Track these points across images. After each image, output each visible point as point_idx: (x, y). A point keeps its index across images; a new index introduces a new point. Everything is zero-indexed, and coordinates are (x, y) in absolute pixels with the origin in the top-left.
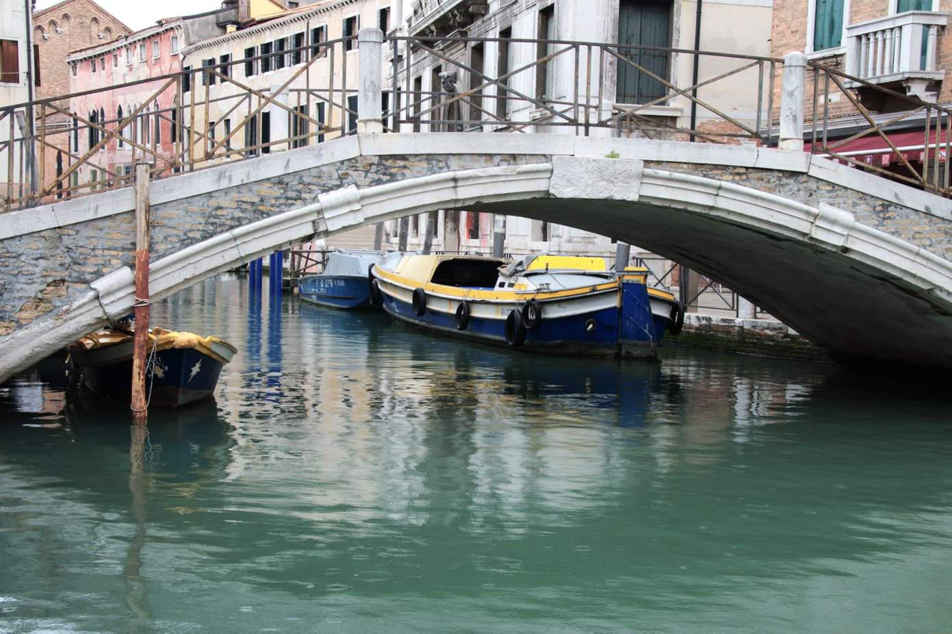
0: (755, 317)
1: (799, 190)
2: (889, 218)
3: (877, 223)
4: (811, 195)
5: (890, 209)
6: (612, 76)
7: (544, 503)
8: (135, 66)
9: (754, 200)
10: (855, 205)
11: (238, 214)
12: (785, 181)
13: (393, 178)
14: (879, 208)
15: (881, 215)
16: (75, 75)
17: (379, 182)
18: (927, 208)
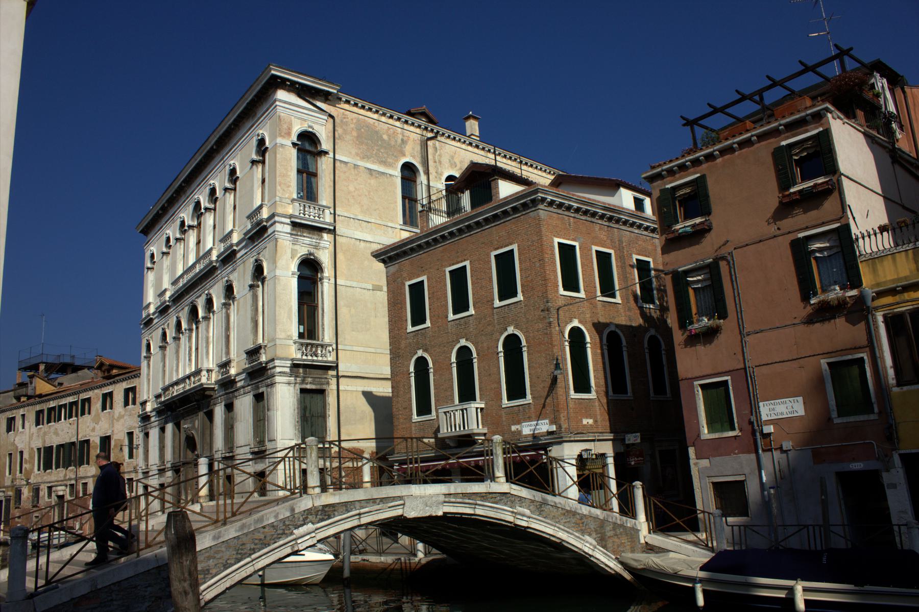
10: (529, 506)
17: (322, 520)
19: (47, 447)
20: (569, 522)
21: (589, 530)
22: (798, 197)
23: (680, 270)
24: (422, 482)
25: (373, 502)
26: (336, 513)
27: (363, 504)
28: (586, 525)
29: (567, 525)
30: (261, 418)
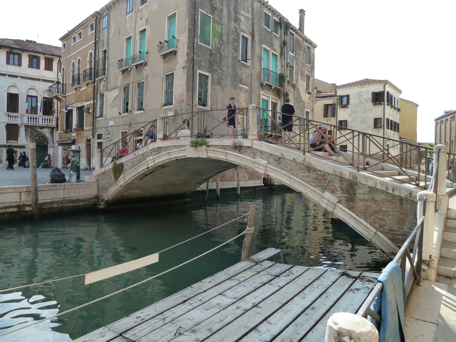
0: (29, 167)
1: (251, 153)
2: (280, 163)
3: (276, 165)
4: (254, 154)
5: (281, 159)
7: (118, 238)
9: (276, 172)
10: (269, 158)
12: (246, 150)
14: (277, 159)
15: (278, 162)
17: (157, 154)
18: (294, 159)
19: (51, 115)
20: (308, 176)
21: (332, 188)
22: (140, 192)
23: (262, 61)
24: (81, 309)
25: (175, 147)
26: (162, 152)
27: (172, 148)
28: (329, 182)
29: (306, 179)
30: (264, 169)
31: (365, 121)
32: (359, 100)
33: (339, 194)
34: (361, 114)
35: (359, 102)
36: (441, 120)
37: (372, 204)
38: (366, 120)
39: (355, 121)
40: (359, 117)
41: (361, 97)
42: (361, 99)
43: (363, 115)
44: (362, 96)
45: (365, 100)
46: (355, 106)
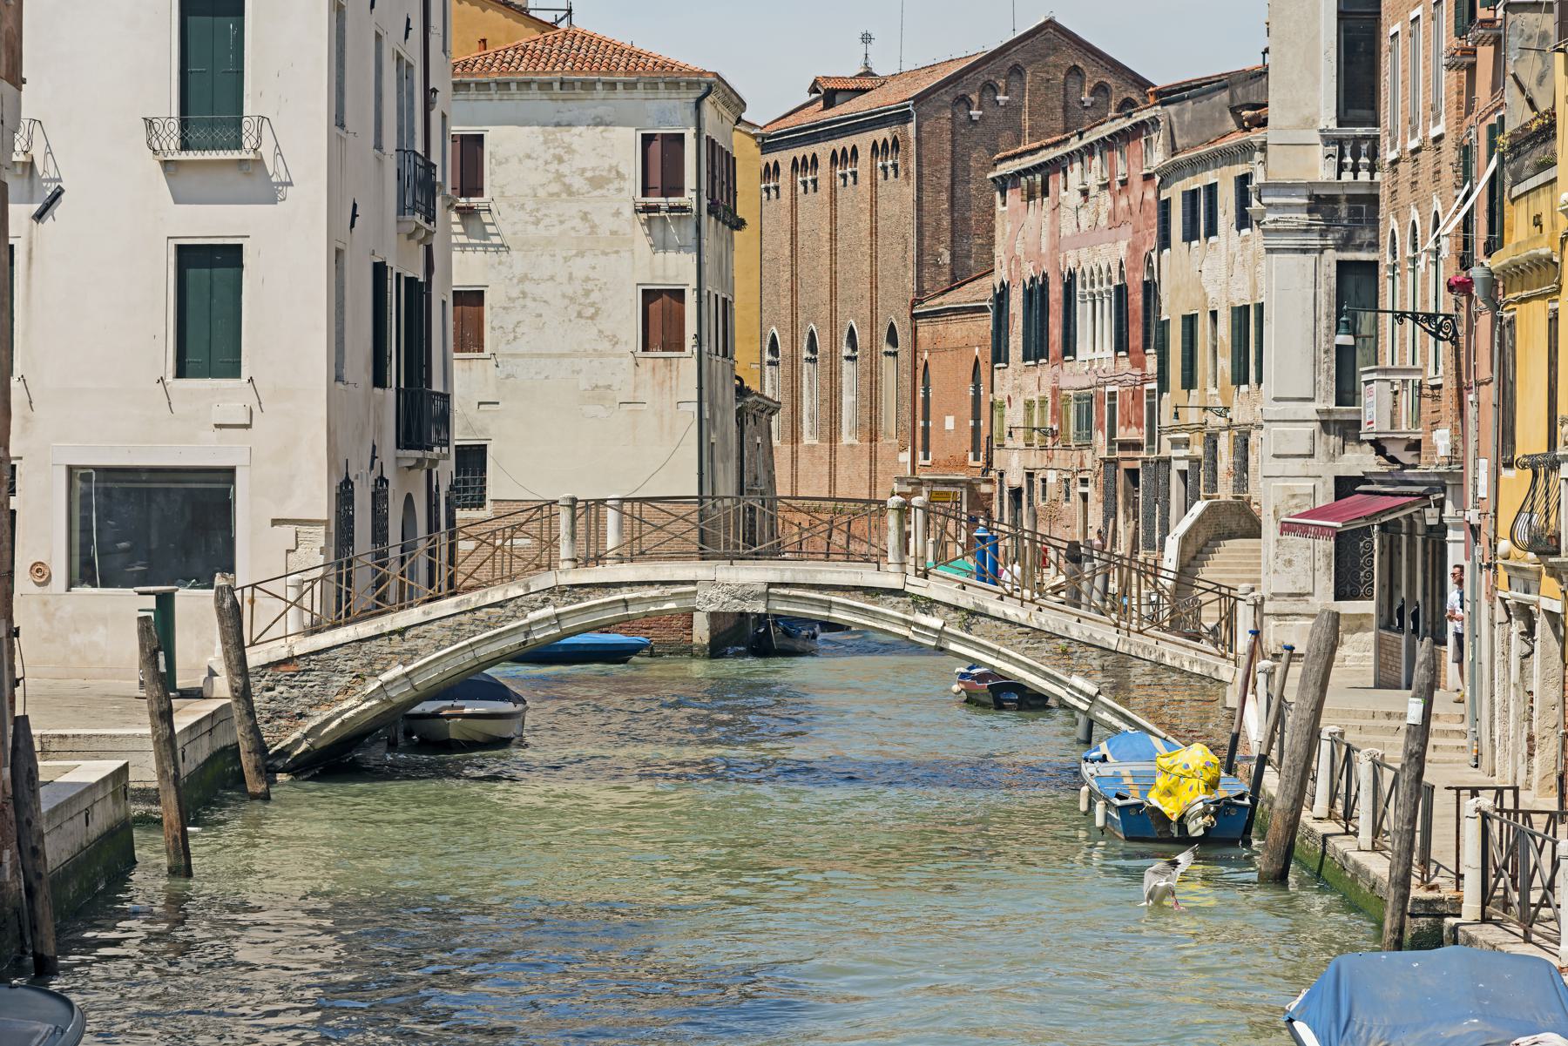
6: (1329, 368)
8: (1091, 193)
11: (473, 628)
13: (581, 600)
16: (1004, 204)
17: (571, 603)
21: (1086, 668)
31: (593, 304)
32: (551, 176)
33: (1099, 676)
34: (566, 259)
35: (555, 188)
36: (806, 151)
37: (1157, 691)
38: (596, 296)
39: (529, 302)
40: (552, 278)
41: (566, 157)
42: (564, 169)
43: (580, 267)
44: (570, 150)
45: (589, 174)
46: (530, 205)
